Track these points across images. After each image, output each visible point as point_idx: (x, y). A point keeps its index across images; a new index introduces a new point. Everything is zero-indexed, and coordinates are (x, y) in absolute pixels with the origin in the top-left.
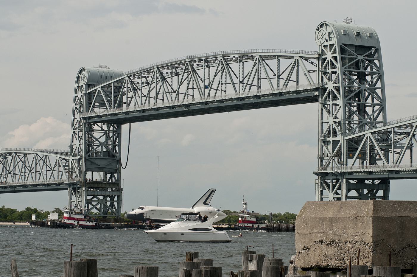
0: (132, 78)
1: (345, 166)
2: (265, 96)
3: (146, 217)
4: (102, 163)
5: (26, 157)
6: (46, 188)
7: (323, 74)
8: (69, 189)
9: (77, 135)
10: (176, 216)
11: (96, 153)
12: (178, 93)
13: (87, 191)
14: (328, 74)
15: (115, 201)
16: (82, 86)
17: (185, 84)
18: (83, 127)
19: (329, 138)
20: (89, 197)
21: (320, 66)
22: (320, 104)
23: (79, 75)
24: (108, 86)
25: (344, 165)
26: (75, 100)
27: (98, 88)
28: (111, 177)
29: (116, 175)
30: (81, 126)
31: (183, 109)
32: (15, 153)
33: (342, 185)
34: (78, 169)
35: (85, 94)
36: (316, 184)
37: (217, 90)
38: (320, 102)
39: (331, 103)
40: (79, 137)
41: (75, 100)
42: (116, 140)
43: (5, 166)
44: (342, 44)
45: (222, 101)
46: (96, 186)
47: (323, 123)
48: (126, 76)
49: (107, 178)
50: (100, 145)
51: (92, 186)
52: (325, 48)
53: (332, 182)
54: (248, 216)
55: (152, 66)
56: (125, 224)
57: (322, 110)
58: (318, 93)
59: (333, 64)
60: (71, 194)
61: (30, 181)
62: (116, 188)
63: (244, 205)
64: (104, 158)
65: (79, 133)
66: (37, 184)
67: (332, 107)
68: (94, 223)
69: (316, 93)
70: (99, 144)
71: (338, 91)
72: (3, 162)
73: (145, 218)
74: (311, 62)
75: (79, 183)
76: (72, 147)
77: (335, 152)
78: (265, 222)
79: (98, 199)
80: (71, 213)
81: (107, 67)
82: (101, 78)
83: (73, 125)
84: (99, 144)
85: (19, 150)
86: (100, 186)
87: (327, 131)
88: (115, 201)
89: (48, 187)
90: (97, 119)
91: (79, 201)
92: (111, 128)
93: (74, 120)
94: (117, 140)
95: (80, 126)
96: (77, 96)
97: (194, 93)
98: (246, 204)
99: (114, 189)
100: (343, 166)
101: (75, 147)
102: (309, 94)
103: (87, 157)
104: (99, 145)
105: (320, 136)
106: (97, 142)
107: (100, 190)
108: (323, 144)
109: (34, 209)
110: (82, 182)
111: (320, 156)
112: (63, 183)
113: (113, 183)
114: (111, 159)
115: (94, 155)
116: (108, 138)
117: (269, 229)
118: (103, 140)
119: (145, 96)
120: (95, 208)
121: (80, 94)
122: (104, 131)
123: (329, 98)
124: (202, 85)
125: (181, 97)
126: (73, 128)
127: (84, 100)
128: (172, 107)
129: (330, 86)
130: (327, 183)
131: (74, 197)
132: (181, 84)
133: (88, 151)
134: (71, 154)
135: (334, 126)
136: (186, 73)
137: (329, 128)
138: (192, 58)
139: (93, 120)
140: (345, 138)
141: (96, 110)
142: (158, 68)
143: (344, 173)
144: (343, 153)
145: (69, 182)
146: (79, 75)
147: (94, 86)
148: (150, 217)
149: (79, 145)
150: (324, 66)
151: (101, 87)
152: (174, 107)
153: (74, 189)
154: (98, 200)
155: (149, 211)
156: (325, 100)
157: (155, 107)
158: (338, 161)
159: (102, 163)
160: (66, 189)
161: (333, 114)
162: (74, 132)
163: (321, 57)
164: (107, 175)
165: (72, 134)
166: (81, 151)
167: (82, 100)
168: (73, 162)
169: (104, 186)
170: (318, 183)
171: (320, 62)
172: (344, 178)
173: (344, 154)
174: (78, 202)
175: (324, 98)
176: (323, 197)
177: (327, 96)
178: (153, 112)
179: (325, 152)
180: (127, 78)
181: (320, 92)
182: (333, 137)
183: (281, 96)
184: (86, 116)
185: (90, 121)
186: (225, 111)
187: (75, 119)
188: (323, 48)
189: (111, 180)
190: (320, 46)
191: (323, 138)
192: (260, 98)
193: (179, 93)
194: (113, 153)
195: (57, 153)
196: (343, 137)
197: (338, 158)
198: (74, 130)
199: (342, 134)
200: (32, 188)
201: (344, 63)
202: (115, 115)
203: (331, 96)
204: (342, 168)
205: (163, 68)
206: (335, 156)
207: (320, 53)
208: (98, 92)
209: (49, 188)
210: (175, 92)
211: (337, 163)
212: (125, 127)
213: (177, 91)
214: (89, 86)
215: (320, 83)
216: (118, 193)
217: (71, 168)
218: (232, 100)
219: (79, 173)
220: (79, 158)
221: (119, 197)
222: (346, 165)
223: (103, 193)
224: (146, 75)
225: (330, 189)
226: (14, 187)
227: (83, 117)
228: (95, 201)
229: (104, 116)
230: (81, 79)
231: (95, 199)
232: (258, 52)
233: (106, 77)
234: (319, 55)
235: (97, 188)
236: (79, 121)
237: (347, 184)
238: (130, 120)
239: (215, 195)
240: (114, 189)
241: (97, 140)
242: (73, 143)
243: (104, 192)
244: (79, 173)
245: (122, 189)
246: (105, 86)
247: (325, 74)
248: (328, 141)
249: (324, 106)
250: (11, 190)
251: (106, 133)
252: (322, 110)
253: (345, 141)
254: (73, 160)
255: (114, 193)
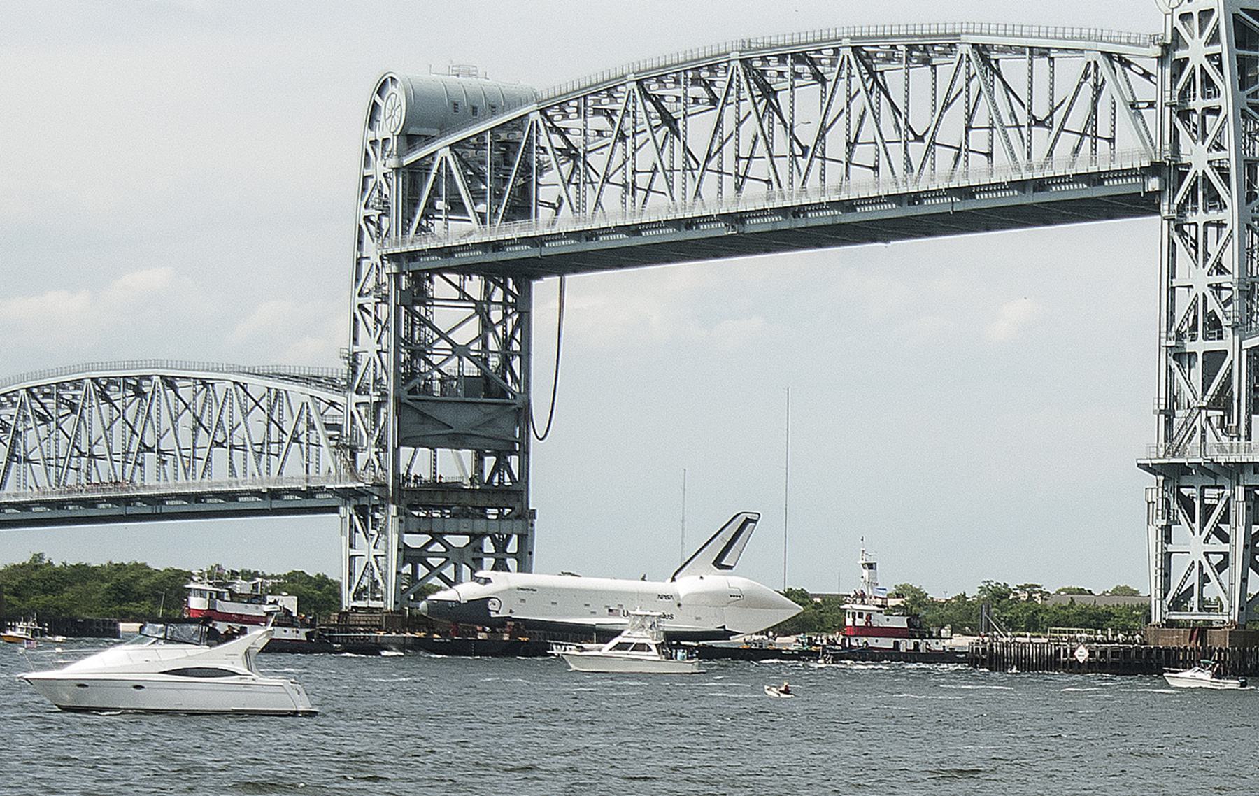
0: (554, 113)
1: (1243, 440)
2: (1118, 177)
3: (497, 612)
4: (463, 419)
5: (211, 393)
6: (117, 510)
7: (1178, 115)
8: (342, 509)
9: (368, 312)
10: (610, 610)
11: (442, 381)
12: (933, 143)
13: (403, 517)
14: (1194, 115)
15: (512, 555)
16: (386, 140)
17: (957, 112)
18: (389, 288)
19: (1194, 341)
20: (416, 541)
21: (1168, 87)
22: (1166, 222)
23: (378, 99)
24: (474, 140)
25: (1239, 440)
26: (364, 189)
27: (441, 148)
28: (496, 469)
29: (514, 461)
30: (384, 284)
31: (721, 229)
32: (161, 377)
33: (1232, 509)
34: (375, 438)
35: (397, 170)
36: (1149, 503)
37: (648, 190)
38: (1165, 214)
39: (1200, 217)
40: (377, 320)
41: (364, 189)
42: (513, 337)
43: (275, 417)
44: (1242, 9)
45: (1094, 179)
46: (439, 499)
47: (1174, 288)
48: (535, 106)
49: (482, 471)
50: (453, 352)
51: (424, 499)
52: (1183, 24)
53: (1202, 497)
54: (878, 612)
55: (619, 74)
56: (418, 635)
57: (1172, 244)
58: (1160, 184)
59: (1208, 82)
60: (351, 527)
61: (219, 479)
62: (513, 509)
63: (866, 573)
64: (467, 400)
65: (376, 309)
66: (166, 495)
67: (1205, 233)
68: (303, 631)
69: (1154, 184)
70: (450, 350)
71: (1225, 177)
72: (264, 404)
73: (493, 615)
74: (1144, 71)
75: (376, 491)
76: (355, 360)
77: (1210, 392)
78: (943, 631)
79: (447, 546)
80: (214, 597)
81: (481, 74)
82: (455, 111)
83: (357, 280)
84: (450, 350)
85: (196, 368)
86: (453, 498)
87: (1187, 319)
88: (512, 555)
89: (273, 501)
90: (437, 262)
91: (377, 552)
92: (498, 295)
93: (359, 263)
94: (518, 336)
95: (378, 286)
96: (371, 176)
97: (1114, 131)
98: (871, 566)
99: (507, 511)
100: (1235, 439)
101: (363, 360)
102: (1130, 186)
103: (405, 397)
104: (450, 353)
105: (1164, 335)
106: (443, 344)
107: (453, 516)
108: (1174, 364)
109: (318, 575)
110: (386, 486)
111: (1162, 407)
112: (321, 490)
113: (502, 490)
114: (495, 404)
115: (437, 386)
116: (487, 325)
117: (977, 659)
118: (468, 333)
119: (805, 150)
120: (436, 578)
121: (379, 168)
122: (473, 305)
123: (1195, 201)
124: (1023, 118)
125: (944, 157)
126: (357, 292)
127: (394, 192)
128: (1031, 184)
129: (1197, 156)
130: (1187, 503)
131: (360, 536)
132: (947, 105)
133: (407, 376)
134: (350, 386)
135: (1212, 305)
136: (732, 103)
137: (1196, 300)
138: (750, 49)
139: (424, 263)
140: (1243, 342)
141: (438, 226)
142: (639, 82)
143: (1241, 467)
144: (1236, 396)
145: (343, 486)
146: (378, 99)
147: (429, 139)
148: (511, 612)
149: (378, 352)
150: (1179, 86)
151: (451, 147)
152: (915, 198)
153: (361, 511)
154: (447, 550)
155: (510, 589)
156: (1182, 208)
157: (844, 197)
158: (1222, 426)
159: (463, 419)
160: (334, 510)
161: (1207, 255)
162: (361, 306)
163: (1169, 49)
164: (482, 459)
165: (354, 314)
166: (384, 374)
167: (386, 190)
168: (359, 412)
169: (466, 499)
170: (1154, 500)
171: (1168, 71)
172: (1238, 485)
173: (1239, 401)
174: (375, 556)
175: (1177, 201)
176: (1170, 548)
177: (1188, 196)
178: (1082, 191)
179: (1179, 391)
180: (536, 116)
181: (1166, 180)
182: (1205, 339)
183: (1040, 191)
184: (397, 250)
185: (415, 266)
186: (874, 240)
187: (362, 258)
188: (1178, 24)
189: (496, 479)
190: (1169, 17)
191: (1173, 343)
192: (1101, 182)
193: (935, 144)
194: (503, 382)
195: (308, 380)
196: (1237, 338)
197: (1221, 413)
198: (362, 300)
199: (1234, 328)
200: (221, 505)
201: (1251, 77)
202: (497, 246)
203: (1200, 194)
204: (1235, 450)
205: (659, 79)
206: (1213, 405)
207: (1169, 41)
208: (441, 164)
209: (276, 504)
210: (919, 139)
211: (1219, 431)
212: (544, 289)
213: (927, 138)
214: (410, 139)
215: (1168, 147)
216: (519, 524)
217: (352, 436)
218: (1065, 183)
219: (376, 453)
220: (376, 399)
221: (525, 539)
222: (1246, 437)
223: (465, 524)
224: (606, 103)
225: (1193, 521)
226: (159, 500)
227: (390, 251)
228: (436, 555)
229: (649, 229)
230: (382, 116)
231: (438, 547)
232: (967, 33)
233: (474, 109)
234: (1165, 47)
235: (441, 508)
236: (377, 266)
237: (1251, 504)
238: (564, 265)
239: (756, 535)
240: (507, 511)
241: (443, 336)
242: (357, 345)
243: (467, 520)
244: (376, 453)
245: (534, 510)
246: (467, 140)
247: (1184, 114)
248: (1189, 353)
249: (1179, 228)
250: (148, 510)
251: (482, 309)
252: (1172, 244)
253: (1244, 353)
254: (357, 405)
255: (506, 526)
